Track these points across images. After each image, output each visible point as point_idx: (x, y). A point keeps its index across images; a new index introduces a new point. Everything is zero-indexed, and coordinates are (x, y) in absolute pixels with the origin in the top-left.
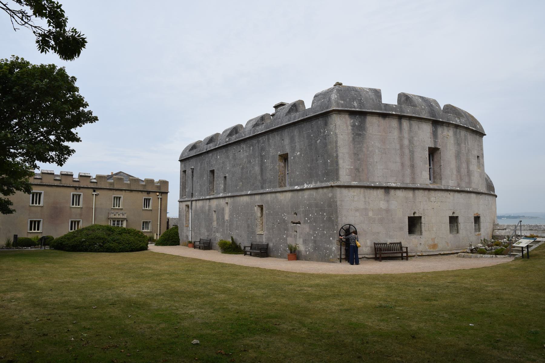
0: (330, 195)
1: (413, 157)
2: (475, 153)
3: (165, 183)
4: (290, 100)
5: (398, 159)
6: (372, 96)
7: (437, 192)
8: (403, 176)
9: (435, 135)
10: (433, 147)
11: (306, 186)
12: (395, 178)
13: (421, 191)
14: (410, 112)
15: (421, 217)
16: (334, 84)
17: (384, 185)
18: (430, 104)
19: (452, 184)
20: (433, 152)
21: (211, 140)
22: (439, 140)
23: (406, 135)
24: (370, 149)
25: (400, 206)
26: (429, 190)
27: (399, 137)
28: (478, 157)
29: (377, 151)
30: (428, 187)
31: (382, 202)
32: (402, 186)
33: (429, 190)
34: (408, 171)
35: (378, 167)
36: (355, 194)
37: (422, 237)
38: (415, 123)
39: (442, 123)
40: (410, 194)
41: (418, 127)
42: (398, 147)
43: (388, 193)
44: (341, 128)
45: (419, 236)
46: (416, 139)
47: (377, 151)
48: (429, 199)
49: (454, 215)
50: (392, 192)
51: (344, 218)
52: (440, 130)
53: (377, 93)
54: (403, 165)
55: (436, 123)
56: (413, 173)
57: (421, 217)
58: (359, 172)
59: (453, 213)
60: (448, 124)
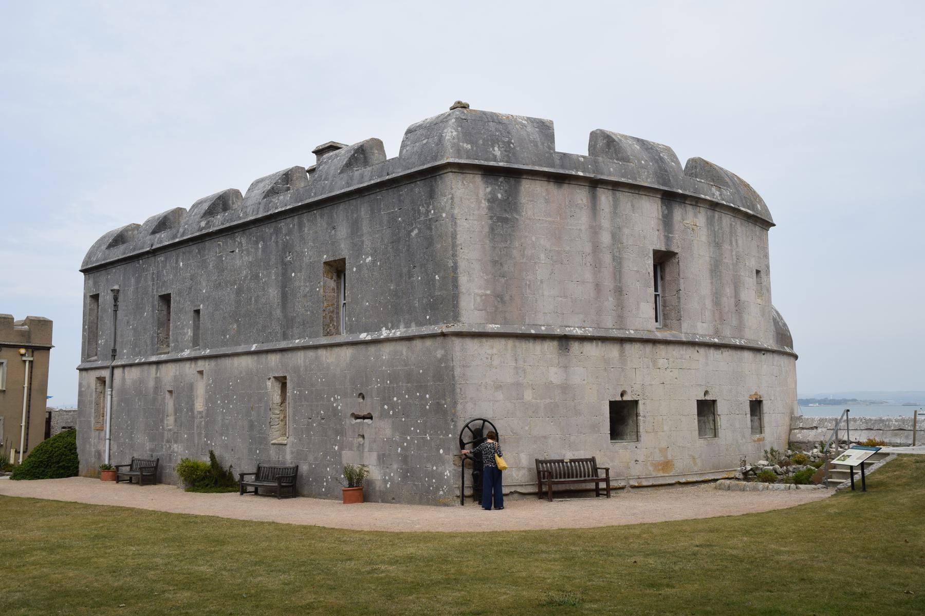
0: (439, 354)
1: (620, 272)
2: (753, 263)
3: (44, 325)
4: (350, 138)
5: (588, 276)
6: (535, 135)
7: (670, 348)
8: (599, 312)
9: (667, 222)
10: (663, 249)
11: (385, 333)
12: (582, 316)
13: (637, 346)
14: (611, 174)
15: (636, 402)
16: (452, 105)
17: (558, 331)
18: (657, 156)
19: (702, 330)
20: (663, 260)
21: (163, 223)
22: (677, 236)
23: (605, 223)
24: (528, 252)
25: (593, 379)
26: (654, 342)
27: (591, 227)
28: (758, 272)
29: (542, 256)
30: (652, 337)
31: (553, 370)
32: (597, 334)
33: (654, 342)
34: (610, 302)
35: (546, 293)
36: (495, 351)
37: (639, 445)
38: (625, 198)
39: (682, 199)
40: (613, 351)
41: (632, 205)
42: (588, 248)
43: (567, 349)
44: (465, 204)
45: (632, 445)
46: (626, 231)
47: (542, 256)
48: (654, 362)
49: (708, 398)
50: (575, 346)
51: (470, 406)
52: (678, 213)
53: (545, 129)
54: (598, 287)
55: (670, 198)
56: (620, 306)
57: (636, 402)
58: (503, 301)
59: (706, 393)
60: (696, 201)
